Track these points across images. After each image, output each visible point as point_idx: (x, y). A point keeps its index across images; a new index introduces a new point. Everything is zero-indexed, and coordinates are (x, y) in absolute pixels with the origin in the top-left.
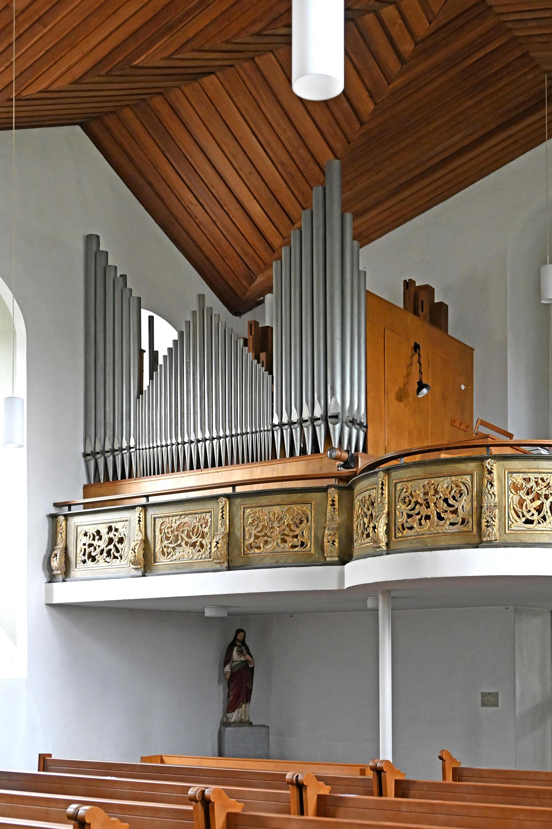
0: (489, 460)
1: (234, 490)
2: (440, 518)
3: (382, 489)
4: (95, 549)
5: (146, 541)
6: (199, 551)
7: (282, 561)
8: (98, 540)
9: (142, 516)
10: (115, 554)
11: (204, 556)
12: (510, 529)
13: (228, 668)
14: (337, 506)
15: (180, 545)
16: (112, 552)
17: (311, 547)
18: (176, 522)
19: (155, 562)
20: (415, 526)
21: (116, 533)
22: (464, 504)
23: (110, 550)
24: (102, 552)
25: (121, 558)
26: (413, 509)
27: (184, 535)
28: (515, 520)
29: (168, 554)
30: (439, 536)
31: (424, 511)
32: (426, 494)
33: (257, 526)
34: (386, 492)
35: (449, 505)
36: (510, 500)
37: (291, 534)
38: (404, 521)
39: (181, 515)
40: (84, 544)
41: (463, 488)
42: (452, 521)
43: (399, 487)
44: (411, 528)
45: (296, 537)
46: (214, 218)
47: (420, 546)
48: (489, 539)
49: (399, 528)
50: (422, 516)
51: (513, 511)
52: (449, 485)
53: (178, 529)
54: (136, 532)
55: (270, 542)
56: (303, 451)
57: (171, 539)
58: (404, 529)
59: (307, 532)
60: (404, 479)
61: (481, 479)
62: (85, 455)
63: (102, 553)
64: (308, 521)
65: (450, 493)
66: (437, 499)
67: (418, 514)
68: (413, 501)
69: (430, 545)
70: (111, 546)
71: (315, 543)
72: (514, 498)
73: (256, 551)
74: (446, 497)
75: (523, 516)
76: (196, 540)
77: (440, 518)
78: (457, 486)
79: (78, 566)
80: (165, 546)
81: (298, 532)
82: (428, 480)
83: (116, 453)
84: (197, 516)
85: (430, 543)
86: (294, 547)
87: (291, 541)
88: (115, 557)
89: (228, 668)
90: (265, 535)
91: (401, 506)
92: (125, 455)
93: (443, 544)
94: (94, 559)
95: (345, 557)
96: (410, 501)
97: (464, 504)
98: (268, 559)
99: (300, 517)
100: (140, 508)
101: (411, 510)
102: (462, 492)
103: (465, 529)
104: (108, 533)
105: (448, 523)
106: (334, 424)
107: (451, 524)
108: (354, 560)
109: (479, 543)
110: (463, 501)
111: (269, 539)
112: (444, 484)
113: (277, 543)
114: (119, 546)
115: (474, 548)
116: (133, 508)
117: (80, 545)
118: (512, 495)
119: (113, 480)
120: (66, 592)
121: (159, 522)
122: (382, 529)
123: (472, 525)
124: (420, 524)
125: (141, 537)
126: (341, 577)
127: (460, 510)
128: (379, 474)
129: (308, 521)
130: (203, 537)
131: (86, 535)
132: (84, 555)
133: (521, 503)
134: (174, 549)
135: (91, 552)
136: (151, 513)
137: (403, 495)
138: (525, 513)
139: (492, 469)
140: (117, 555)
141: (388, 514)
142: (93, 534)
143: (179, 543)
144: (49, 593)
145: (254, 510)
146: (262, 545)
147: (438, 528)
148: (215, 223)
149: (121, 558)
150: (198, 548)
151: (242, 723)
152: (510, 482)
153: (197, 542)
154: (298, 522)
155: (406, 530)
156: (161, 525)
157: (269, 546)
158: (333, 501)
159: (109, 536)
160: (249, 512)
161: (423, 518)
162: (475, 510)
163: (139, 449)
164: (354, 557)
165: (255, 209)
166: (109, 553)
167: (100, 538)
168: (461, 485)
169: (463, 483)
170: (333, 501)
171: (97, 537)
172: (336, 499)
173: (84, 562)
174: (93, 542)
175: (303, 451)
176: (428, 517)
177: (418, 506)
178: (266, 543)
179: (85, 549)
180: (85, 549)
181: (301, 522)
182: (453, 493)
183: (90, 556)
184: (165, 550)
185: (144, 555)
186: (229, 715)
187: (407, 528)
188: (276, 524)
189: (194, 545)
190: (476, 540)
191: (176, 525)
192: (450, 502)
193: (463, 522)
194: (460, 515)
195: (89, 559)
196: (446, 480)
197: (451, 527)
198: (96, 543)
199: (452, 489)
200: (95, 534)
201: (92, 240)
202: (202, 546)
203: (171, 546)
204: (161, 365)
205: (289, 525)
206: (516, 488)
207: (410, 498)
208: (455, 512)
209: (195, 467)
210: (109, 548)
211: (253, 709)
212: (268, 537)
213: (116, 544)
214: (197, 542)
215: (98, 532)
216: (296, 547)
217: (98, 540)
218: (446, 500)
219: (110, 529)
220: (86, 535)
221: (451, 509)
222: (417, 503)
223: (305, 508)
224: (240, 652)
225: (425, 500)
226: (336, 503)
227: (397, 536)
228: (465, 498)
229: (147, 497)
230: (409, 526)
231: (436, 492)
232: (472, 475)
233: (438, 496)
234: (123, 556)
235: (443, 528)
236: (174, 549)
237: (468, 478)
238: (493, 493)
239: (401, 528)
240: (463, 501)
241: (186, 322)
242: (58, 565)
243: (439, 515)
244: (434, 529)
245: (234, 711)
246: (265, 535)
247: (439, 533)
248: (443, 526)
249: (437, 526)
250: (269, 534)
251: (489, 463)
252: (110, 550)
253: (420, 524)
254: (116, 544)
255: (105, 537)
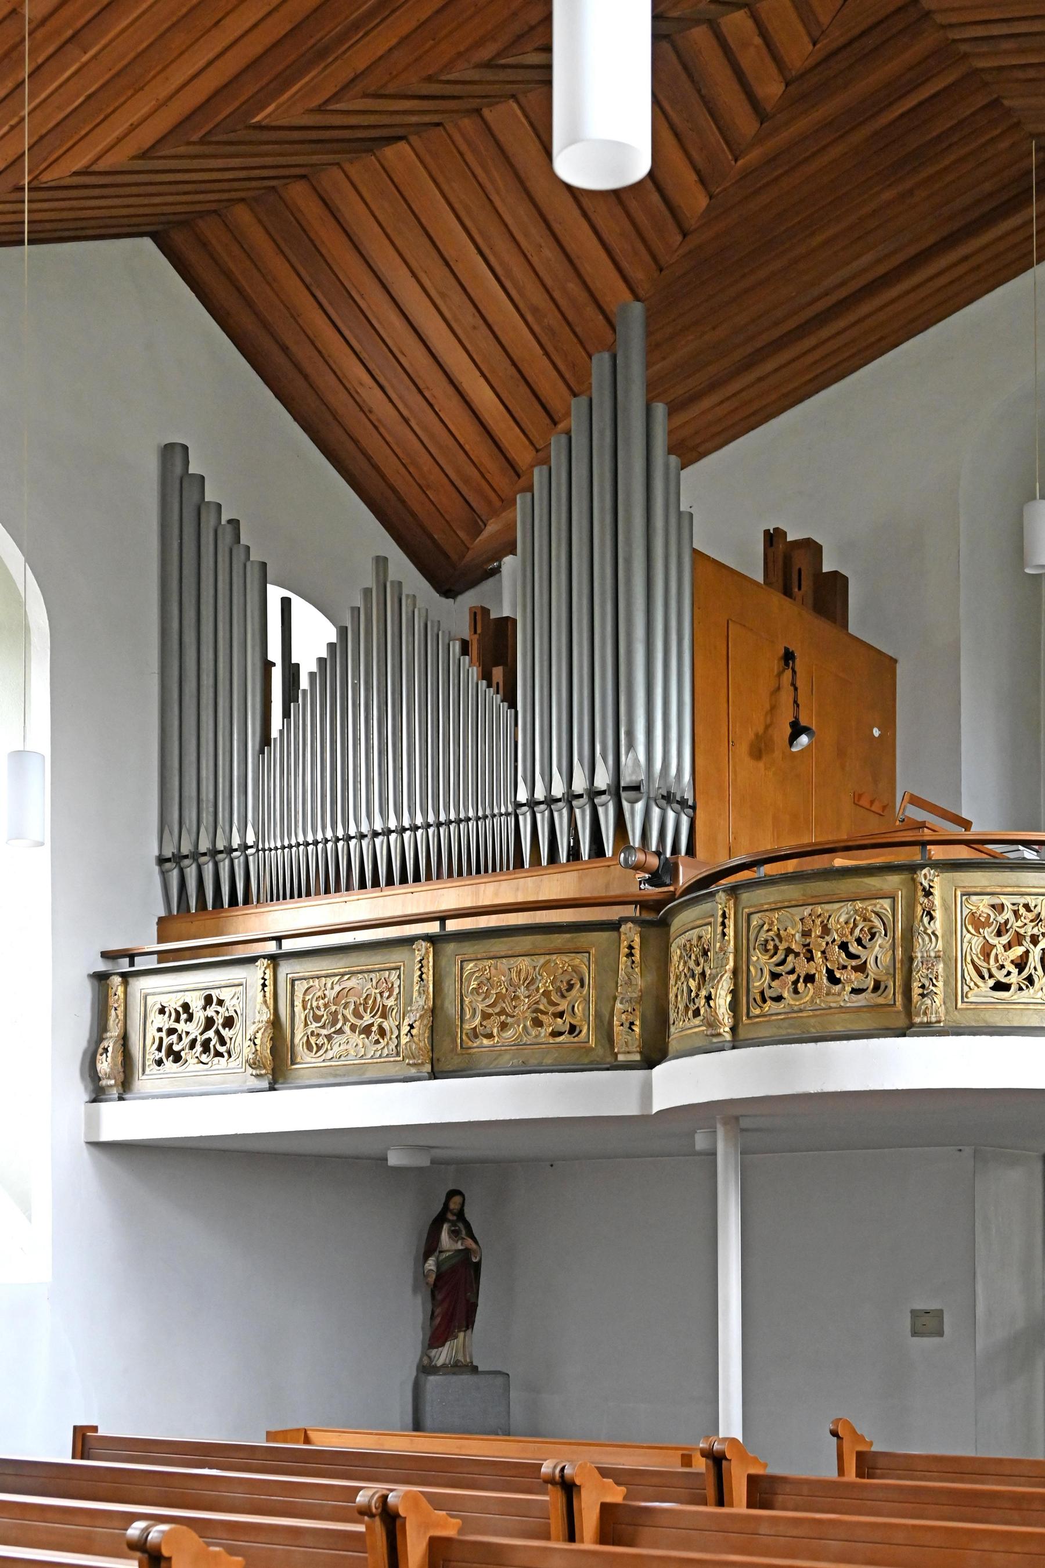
0: (925, 871)
1: (443, 926)
2: (833, 980)
3: (723, 924)
4: (180, 1038)
5: (275, 1023)
6: (377, 1042)
7: (533, 1062)
8: (186, 1021)
9: (269, 975)
10: (218, 1047)
11: (386, 1052)
12: (966, 1000)
13: (431, 1264)
14: (637, 957)
15: (340, 1032)
16: (212, 1043)
17: (589, 1035)
18: (332, 988)
19: (293, 1063)
20: (786, 995)
21: (219, 1008)
22: (878, 954)
23: (209, 1040)
24: (193, 1044)
25: (230, 1056)
26: (782, 963)
27: (348, 1013)
28: (976, 984)
29: (319, 1048)
30: (831, 1014)
31: (803, 967)
32: (806, 934)
33: (487, 995)
34: (730, 931)
35: (851, 956)
36: (965, 945)
37: (552, 1009)
38: (766, 985)
39: (343, 975)
40: (160, 1030)
41: (877, 922)
42: (855, 985)
43: (755, 921)
44: (778, 999)
45: (561, 1015)
46: (405, 413)
47: (796, 1032)
48: (925, 1020)
49: (755, 999)
50: (799, 977)
51: (970, 967)
52: (850, 918)
53: (336, 1000)
54: (258, 1007)
55: (512, 1025)
56: (574, 854)
57: (323, 1020)
58: (764, 1001)
59: (581, 1007)
60: (766, 907)
61: (911, 906)
62: (161, 861)
63: (192, 1046)
64: (582, 986)
65: (852, 933)
66: (827, 943)
67: (792, 972)
68: (782, 947)
69: (814, 1030)
70: (211, 1034)
71: (597, 1027)
72: (973, 942)
73: (485, 1042)
74: (844, 939)
75: (991, 976)
76: (370, 1022)
77: (833, 980)
78: (865, 920)
79: (147, 1071)
80: (312, 1033)
81: (563, 1006)
82: (810, 907)
83: (220, 856)
84: (373, 975)
85: (814, 1027)
86: (556, 1034)
87: (551, 1024)
88: (218, 1054)
89: (431, 1264)
90: (503, 1012)
91: (758, 957)
92: (236, 861)
93: (838, 1028)
94: (177, 1058)
95: (653, 1054)
96: (776, 948)
97: (878, 954)
98: (507, 1057)
99: (568, 978)
100: (266, 962)
101: (778, 965)
102: (874, 930)
103: (881, 1001)
104: (205, 1009)
105: (848, 989)
106: (633, 802)
107: (854, 991)
108: (670, 1060)
109: (907, 1026)
110: (877, 948)
111: (509, 1020)
112: (840, 915)
113: (525, 1027)
114: (226, 1033)
115: (898, 1036)
116: (253, 960)
117: (152, 1032)
118: (969, 936)
119: (214, 908)
120: (125, 1121)
121: (300, 987)
122: (722, 1001)
123: (893, 994)
124: (796, 991)
125: (266, 1015)
126: (646, 1092)
127: (871, 964)
128: (717, 897)
129: (582, 986)
130: (384, 1016)
131: (162, 1011)
132: (159, 1049)
133: (987, 951)
134: (329, 1038)
135: (172, 1044)
136: (286, 969)
137: (763, 936)
138: (994, 971)
139: (931, 887)
140: (222, 1049)
141: (735, 972)
142: (175, 1009)
143: (338, 1026)
144: (93, 1122)
145: (481, 964)
146: (495, 1031)
147: (830, 998)
148: (406, 421)
149: (230, 1056)
150: (374, 1036)
151: (457, 1367)
152: (966, 912)
153: (372, 1024)
154: (564, 987)
155: (769, 1002)
156: (305, 994)
157: (509, 1033)
158: (631, 947)
159: (206, 1013)
160: (471, 969)
161: (801, 980)
162: (898, 965)
163: (264, 850)
164: (671, 1053)
165: (483, 396)
166: (206, 1045)
167: (190, 1018)
168: (874, 918)
169: (877, 914)
170: (631, 947)
171: (184, 1016)
172: (637, 944)
173: (159, 1062)
174: (176, 1025)
175: (574, 854)
176: (810, 978)
177: (790, 958)
178: (504, 1026)
179: (161, 1039)
180: (161, 1039)
181: (571, 987)
182: (857, 932)
183: (170, 1051)
184: (313, 1040)
185: (273, 1050)
186: (433, 1352)
187: (771, 998)
188: (522, 991)
189: (367, 1030)
190: (901, 1022)
191: (334, 993)
192: (852, 949)
193: (876, 988)
194: (872, 975)
195: (168, 1056)
196: (845, 908)
197: (854, 997)
198: (181, 1027)
199: (855, 926)
200: (180, 1009)
201: (173, 455)
202: (382, 1032)
203: (324, 1032)
204: (304, 691)
205: (546, 994)
206: (978, 923)
207: (777, 941)
208: (862, 968)
209: (369, 883)
210: (206, 1036)
211: (480, 1342)
212: (507, 1015)
213: (220, 1028)
214: (372, 1024)
215: (186, 1007)
216: (561, 1034)
217: (186, 1021)
218: (844, 946)
219: (208, 1000)
220: (162, 1011)
221: (854, 963)
222: (789, 951)
223: (578, 960)
224: (455, 1234)
225: (804, 946)
226: (637, 952)
227: (751, 1015)
228: (879, 942)
229: (278, 939)
230: (774, 995)
231: (826, 930)
232: (894, 898)
233: (828, 939)
234: (233, 1052)
235: (838, 999)
236: (329, 1038)
237: (886, 903)
238: (933, 933)
239: (758, 998)
240: (877, 948)
241: (353, 609)
242: (109, 1069)
243: (830, 974)
244: (821, 1001)
245: (443, 1345)
246: (503, 1012)
247: (831, 1008)
248: (839, 994)
249: (827, 994)
250: (509, 1010)
251: (925, 875)
252: (209, 1040)
253: (796, 991)
254: (220, 1028)
255: (200, 1016)
